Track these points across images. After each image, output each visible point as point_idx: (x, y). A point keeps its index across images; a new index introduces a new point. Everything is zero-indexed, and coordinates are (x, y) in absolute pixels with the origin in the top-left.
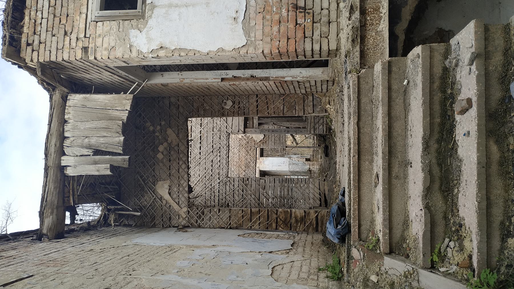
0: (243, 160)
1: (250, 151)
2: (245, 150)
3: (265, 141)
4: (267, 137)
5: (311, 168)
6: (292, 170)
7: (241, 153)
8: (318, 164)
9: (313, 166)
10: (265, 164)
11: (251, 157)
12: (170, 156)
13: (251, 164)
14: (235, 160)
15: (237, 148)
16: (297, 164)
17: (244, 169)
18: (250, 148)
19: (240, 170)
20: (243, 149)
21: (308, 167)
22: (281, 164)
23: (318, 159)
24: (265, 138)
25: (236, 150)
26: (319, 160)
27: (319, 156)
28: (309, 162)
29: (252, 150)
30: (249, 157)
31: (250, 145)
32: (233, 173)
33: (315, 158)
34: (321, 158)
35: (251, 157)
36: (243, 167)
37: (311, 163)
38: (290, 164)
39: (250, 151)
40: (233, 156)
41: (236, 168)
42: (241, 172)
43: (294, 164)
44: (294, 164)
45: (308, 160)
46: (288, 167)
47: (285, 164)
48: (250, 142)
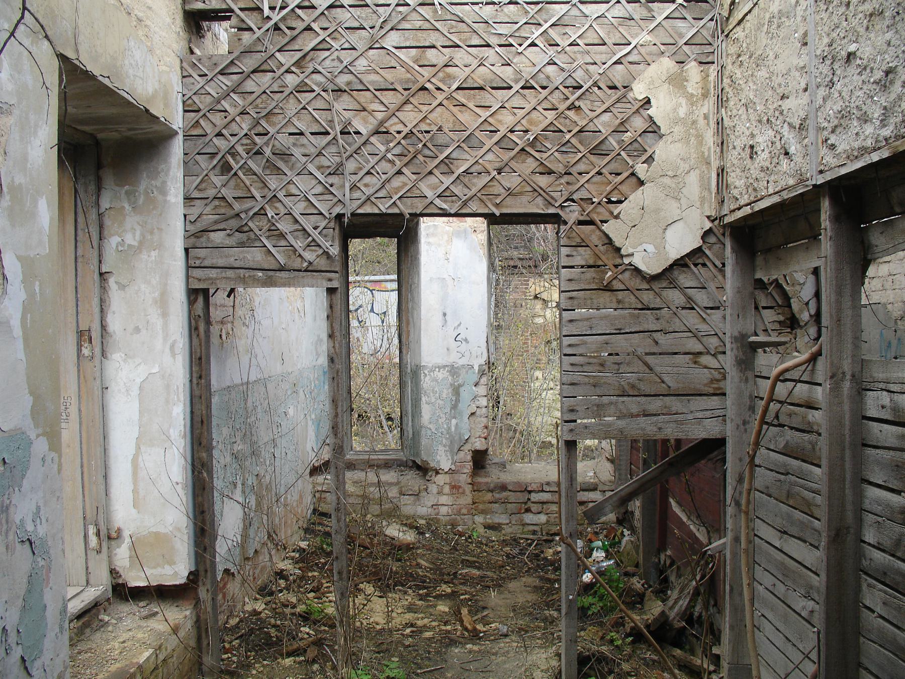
0: (465, 117)
1: (531, 164)
2: (536, 130)
3: (617, 285)
4: (647, 297)
5: (441, 479)
6: (426, 382)
7: (517, 101)
8: (459, 513)
9: (447, 489)
10: (450, 241)
11: (485, 179)
12: (544, 88)
13: (432, 180)
14: (460, 56)
15: (550, 69)
16: (454, 407)
17: (393, 126)
18: (561, 169)
19: (389, 98)
20: (551, 115)
21: (446, 465)
22: (451, 323)
23: (483, 512)
24: (637, 283)
25: (538, 57)
26: (479, 519)
27: (502, 519)
28: (468, 467)
29: (543, 181)
30: (491, 160)
31: (581, 167)
32: (361, 46)
33: (489, 496)
34: (488, 527)
35: (485, 179)
36: (410, 117)
37: (464, 479)
38: (453, 370)
39: (531, 164)
40: (493, 41)
41: (403, 64)
42: (376, 106)
43: (456, 391)
44: (456, 391)
45: (479, 459)
46: (440, 361)
47: (454, 344)
48: (601, 162)
